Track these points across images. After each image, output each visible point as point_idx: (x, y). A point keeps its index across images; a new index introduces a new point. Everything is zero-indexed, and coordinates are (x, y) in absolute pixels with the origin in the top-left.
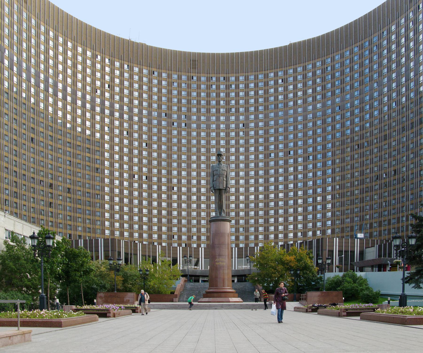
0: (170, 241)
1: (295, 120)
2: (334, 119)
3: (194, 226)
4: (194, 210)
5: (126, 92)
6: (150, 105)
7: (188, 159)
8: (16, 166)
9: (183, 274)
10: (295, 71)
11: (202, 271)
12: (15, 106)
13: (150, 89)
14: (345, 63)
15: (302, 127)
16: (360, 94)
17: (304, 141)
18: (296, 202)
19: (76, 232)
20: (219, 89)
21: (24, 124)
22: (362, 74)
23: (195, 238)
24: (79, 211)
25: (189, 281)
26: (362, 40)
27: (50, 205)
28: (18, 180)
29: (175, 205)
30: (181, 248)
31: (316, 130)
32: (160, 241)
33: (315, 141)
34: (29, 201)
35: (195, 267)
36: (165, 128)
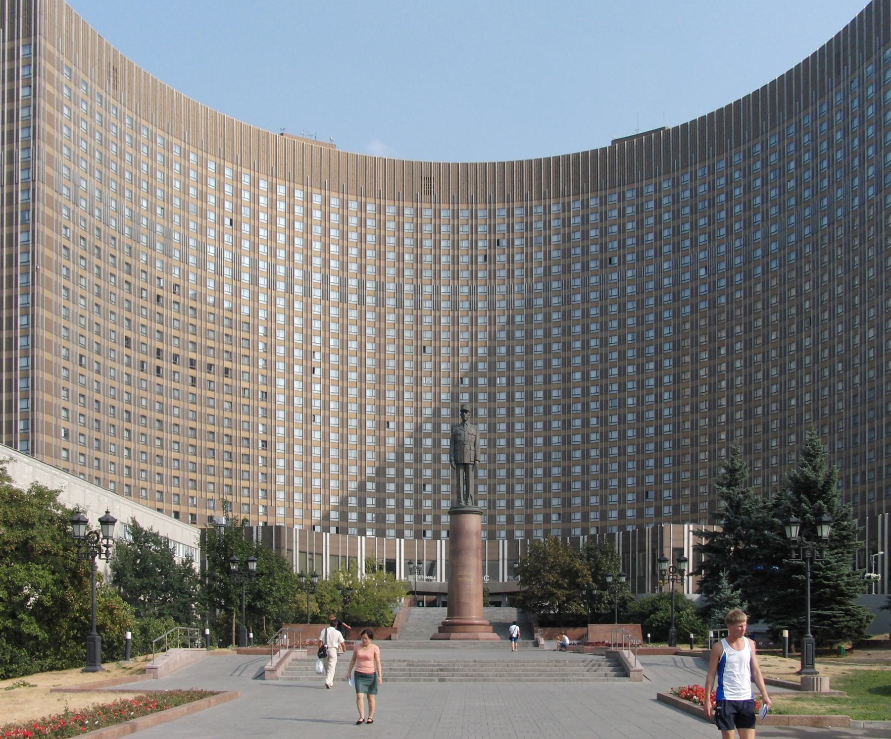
0: (383, 525)
1: (622, 293)
2: (694, 226)
3: (427, 451)
4: (427, 466)
5: (298, 258)
6: (344, 329)
7: (416, 461)
8: (98, 391)
9: (408, 590)
10: (622, 197)
11: (441, 584)
12: (96, 281)
13: (343, 376)
14: (717, 183)
15: (635, 306)
16: (745, 245)
17: (638, 430)
18: (622, 451)
19: (204, 510)
20: (476, 385)
21: (112, 313)
22: (748, 206)
23: (429, 518)
24: (211, 335)
25: (417, 604)
26: (749, 140)
27: (158, 301)
28: (102, 245)
29: (391, 503)
30: (402, 540)
31: (661, 345)
32: (361, 525)
33: (658, 220)
34: (121, 455)
35: (429, 577)
36: (372, 511)
